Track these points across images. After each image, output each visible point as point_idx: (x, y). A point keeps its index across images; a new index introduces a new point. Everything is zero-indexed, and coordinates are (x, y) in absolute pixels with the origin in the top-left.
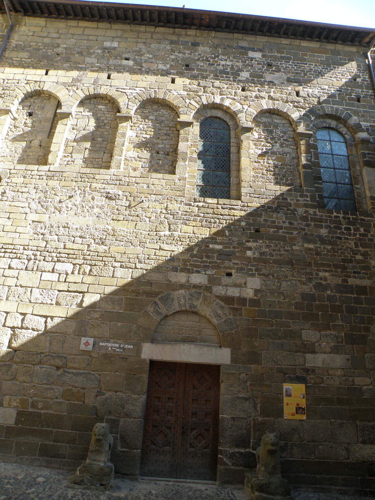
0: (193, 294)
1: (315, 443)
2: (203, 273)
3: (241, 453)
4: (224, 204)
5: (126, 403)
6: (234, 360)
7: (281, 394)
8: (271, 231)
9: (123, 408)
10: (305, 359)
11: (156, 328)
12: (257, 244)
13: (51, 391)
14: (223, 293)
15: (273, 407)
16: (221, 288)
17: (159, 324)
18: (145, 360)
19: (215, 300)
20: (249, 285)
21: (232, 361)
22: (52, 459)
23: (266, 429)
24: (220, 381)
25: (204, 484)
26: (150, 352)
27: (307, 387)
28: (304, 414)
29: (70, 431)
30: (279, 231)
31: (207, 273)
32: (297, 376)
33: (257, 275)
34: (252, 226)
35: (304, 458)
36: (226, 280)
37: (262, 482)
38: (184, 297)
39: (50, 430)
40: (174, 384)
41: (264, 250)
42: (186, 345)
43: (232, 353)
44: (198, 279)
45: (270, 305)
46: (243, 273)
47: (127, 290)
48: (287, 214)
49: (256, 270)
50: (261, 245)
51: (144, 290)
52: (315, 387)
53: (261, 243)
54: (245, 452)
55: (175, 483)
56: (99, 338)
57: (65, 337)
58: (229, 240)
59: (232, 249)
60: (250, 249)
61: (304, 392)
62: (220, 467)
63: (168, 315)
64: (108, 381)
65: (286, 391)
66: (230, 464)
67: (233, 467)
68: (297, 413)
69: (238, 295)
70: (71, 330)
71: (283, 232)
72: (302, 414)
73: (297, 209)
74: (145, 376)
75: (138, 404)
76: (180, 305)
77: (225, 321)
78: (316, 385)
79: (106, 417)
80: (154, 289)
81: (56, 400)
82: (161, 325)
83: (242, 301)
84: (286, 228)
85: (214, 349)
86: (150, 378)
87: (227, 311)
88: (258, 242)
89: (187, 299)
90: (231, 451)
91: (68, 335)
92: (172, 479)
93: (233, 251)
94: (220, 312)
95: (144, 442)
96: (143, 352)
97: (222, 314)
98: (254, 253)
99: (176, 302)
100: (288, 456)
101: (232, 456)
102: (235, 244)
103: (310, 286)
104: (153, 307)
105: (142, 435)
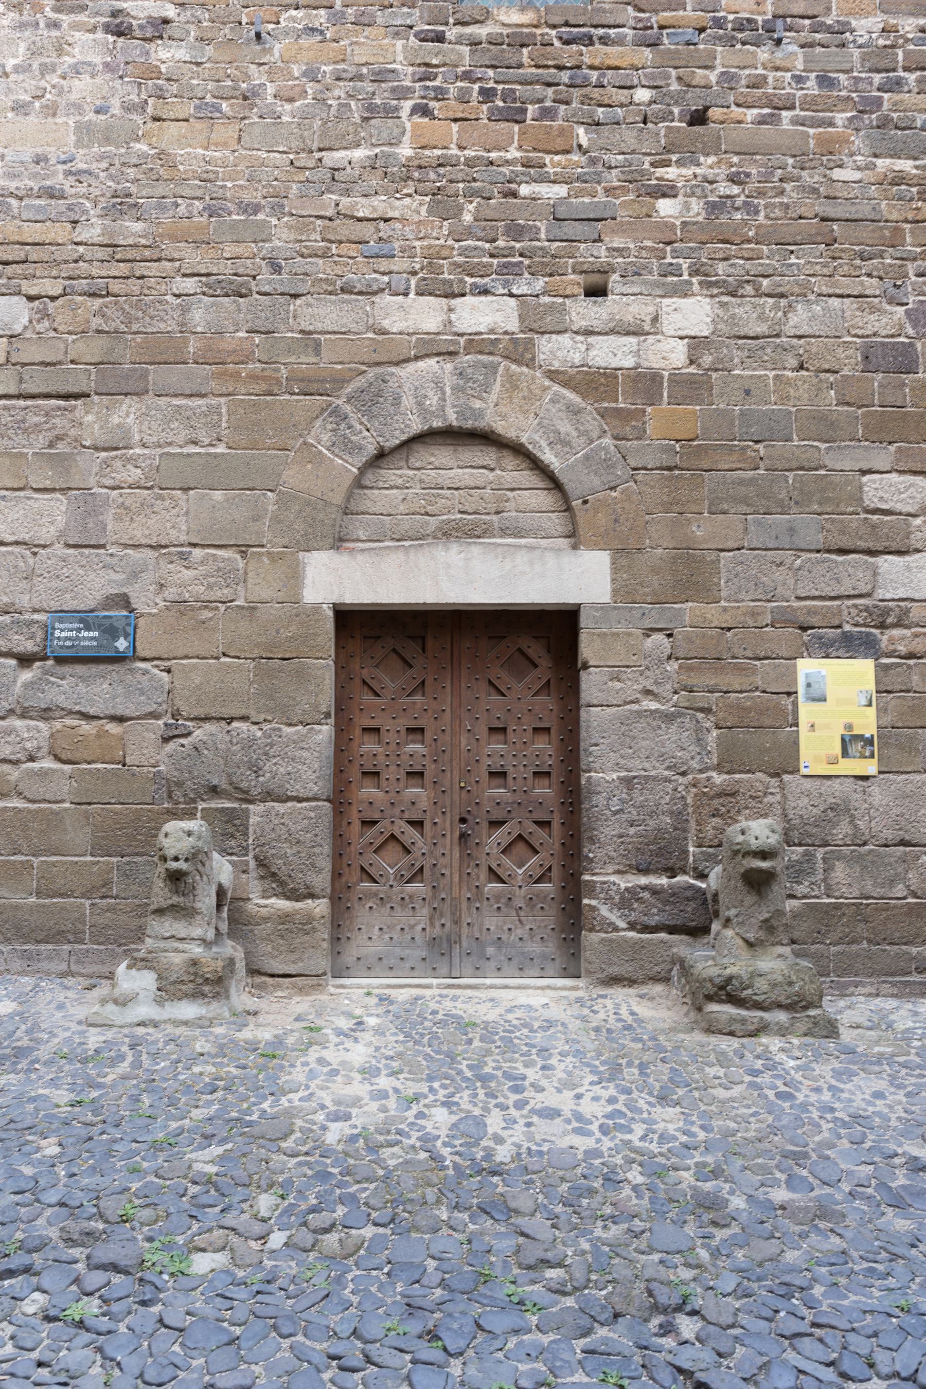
0: (469, 370)
1: (908, 849)
2: (501, 291)
3: (655, 891)
4: (567, 24)
5: (266, 754)
6: (623, 592)
7: (789, 694)
8: (839, 123)
9: (258, 771)
10: (875, 574)
11: (348, 500)
12: (698, 171)
13: (9, 739)
14: (577, 359)
15: (761, 736)
16: (565, 340)
17: (358, 483)
18: (316, 608)
19: (549, 388)
20: (670, 324)
21: (615, 592)
22: (42, 947)
23: (738, 812)
24: (580, 665)
25: (542, 988)
26: (337, 579)
27: (882, 670)
28: (872, 756)
29: (89, 858)
30: (779, 118)
31: (515, 291)
32: (843, 633)
33: (696, 288)
34: (676, 103)
35: (867, 898)
36: (584, 312)
37: (728, 972)
38: (438, 385)
39: (21, 862)
40: (423, 682)
41: (725, 188)
42: (454, 547)
43: (615, 568)
44: (481, 315)
45: (748, 392)
46: (645, 283)
47: (232, 375)
48: (811, 45)
49: (694, 272)
50: (710, 174)
51: (292, 370)
52: (909, 667)
53: (711, 167)
54: (671, 887)
55: (445, 992)
56: (151, 547)
57: (35, 554)
58: (593, 162)
59: (601, 198)
60: (667, 191)
61: (871, 686)
62: (591, 939)
63: (387, 450)
64: (199, 687)
65: (809, 685)
66: (622, 924)
67: (631, 934)
68: (845, 753)
69: (629, 362)
70: (52, 529)
71: (795, 121)
72: (863, 757)
73: (854, 23)
74: (324, 670)
75: (305, 754)
76: (424, 412)
77: (587, 457)
78: (911, 662)
79: (204, 805)
80: (329, 361)
81: (30, 765)
82: (366, 487)
83: (646, 383)
84: (809, 104)
85: (550, 557)
86: (340, 667)
87: (592, 422)
88: (698, 165)
89: (448, 390)
90: (623, 886)
91: (44, 547)
92: (435, 981)
93: (605, 204)
94: (566, 427)
95: (336, 875)
96: (308, 581)
97: (575, 434)
98: (687, 207)
99: (408, 401)
100: (816, 893)
101: (627, 900)
102: (613, 178)
103: (895, 318)
104: (329, 427)
105: (327, 849)
